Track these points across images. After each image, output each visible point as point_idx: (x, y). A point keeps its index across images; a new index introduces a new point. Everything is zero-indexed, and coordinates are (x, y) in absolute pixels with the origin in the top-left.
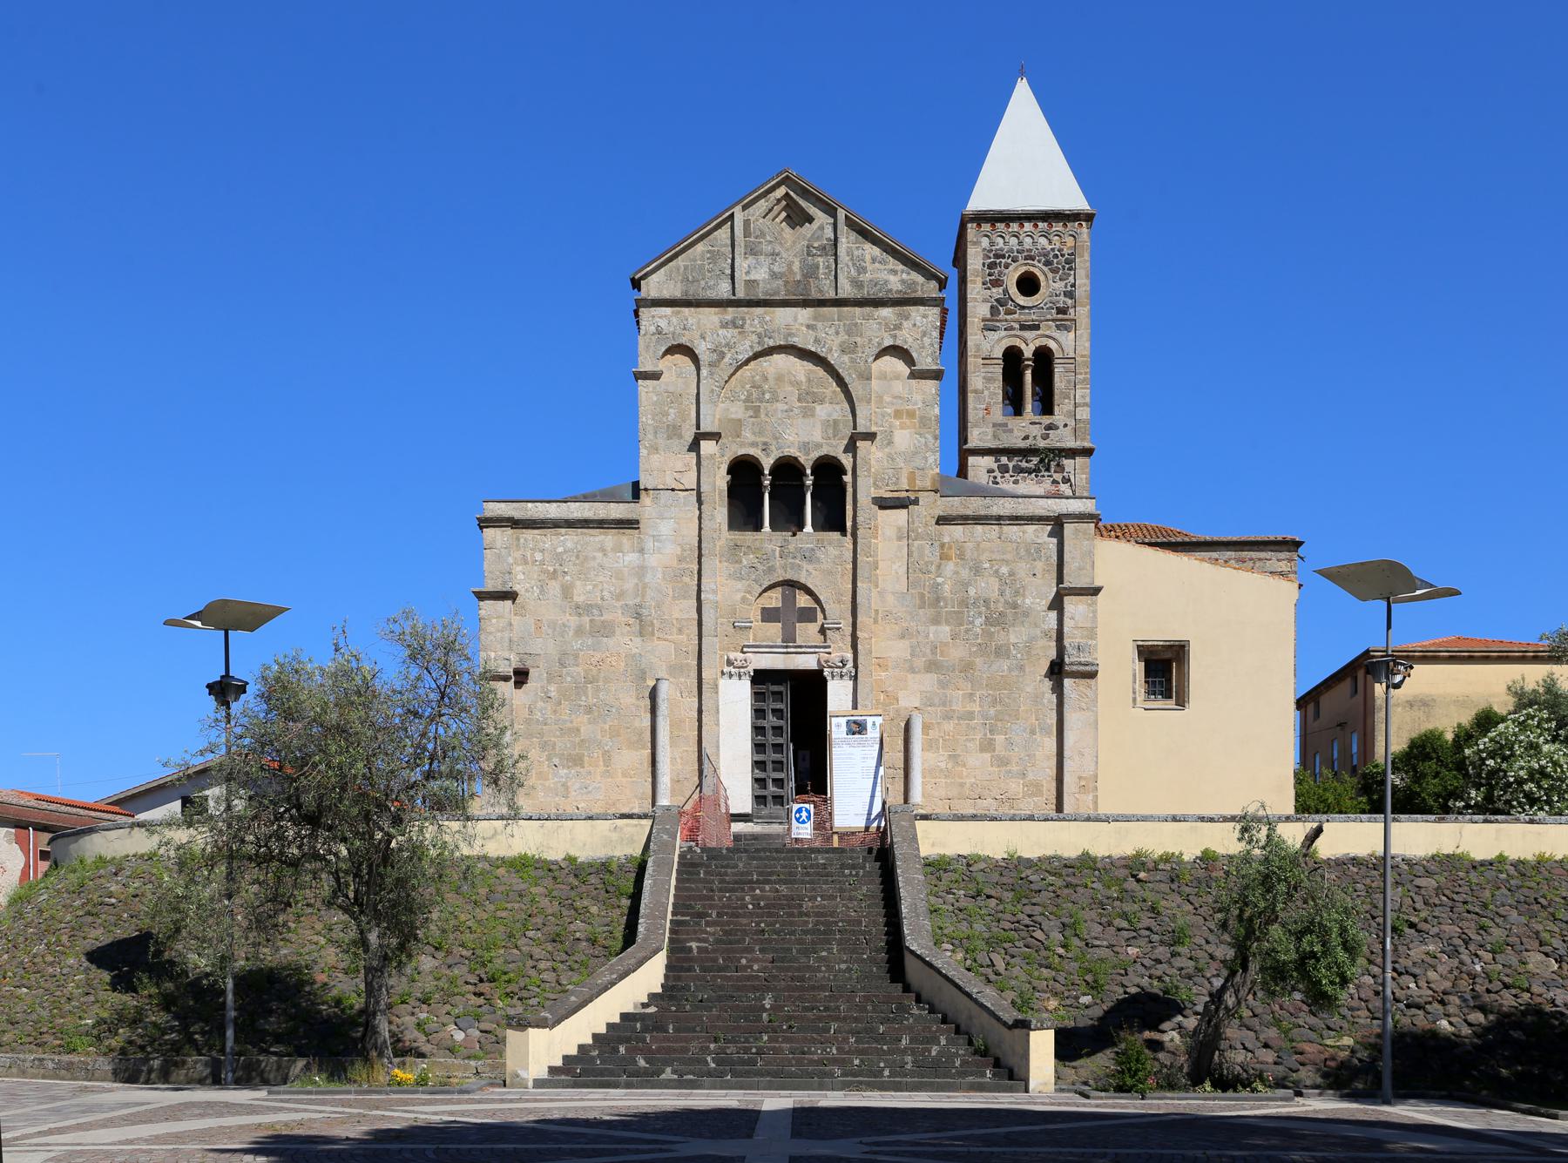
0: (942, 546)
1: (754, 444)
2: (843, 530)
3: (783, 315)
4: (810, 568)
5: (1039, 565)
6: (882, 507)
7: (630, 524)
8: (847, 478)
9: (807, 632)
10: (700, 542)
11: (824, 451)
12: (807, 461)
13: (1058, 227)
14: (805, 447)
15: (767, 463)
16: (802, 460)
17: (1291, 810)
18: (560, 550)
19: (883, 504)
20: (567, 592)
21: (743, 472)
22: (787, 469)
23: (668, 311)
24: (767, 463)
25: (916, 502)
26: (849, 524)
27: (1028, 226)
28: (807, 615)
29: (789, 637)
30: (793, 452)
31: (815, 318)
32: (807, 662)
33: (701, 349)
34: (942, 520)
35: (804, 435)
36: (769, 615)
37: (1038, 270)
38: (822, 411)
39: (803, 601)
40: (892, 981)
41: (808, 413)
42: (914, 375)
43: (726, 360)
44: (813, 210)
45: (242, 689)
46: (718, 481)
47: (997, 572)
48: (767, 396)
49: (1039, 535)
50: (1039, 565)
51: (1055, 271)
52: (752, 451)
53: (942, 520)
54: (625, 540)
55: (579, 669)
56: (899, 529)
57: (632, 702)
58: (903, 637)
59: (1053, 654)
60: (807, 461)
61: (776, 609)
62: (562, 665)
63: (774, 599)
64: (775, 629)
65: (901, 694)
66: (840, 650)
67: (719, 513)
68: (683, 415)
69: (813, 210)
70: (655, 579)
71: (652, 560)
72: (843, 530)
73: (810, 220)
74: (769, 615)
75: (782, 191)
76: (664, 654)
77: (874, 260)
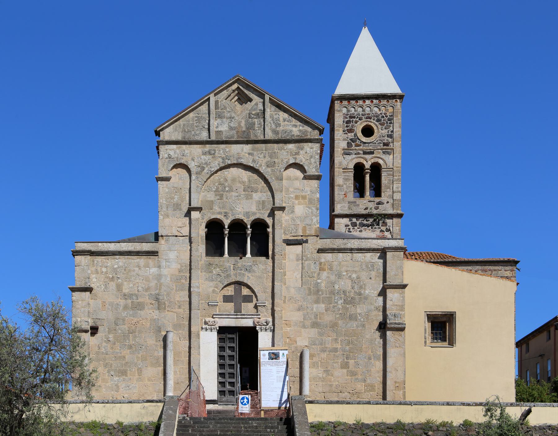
0: (321, 264)
1: (220, 213)
4: (249, 275)
5: (373, 273)
6: (288, 244)
7: (154, 253)
8: (270, 230)
9: (248, 307)
12: (248, 221)
13: (384, 102)
15: (227, 223)
16: (245, 221)
18: (116, 266)
19: (289, 243)
22: (238, 226)
24: (227, 223)
25: (306, 242)
26: (270, 253)
27: (368, 102)
28: (248, 299)
29: (238, 310)
30: (241, 217)
32: (248, 323)
33: (192, 165)
34: (320, 251)
37: (373, 124)
38: (256, 196)
39: (245, 292)
42: (305, 178)
43: (205, 171)
44: (252, 95)
46: (201, 231)
47: (350, 276)
48: (227, 189)
49: (374, 258)
50: (373, 273)
51: (382, 124)
52: (218, 217)
53: (320, 251)
55: (125, 326)
57: (153, 342)
58: (299, 310)
59: (381, 318)
60: (248, 221)
61: (231, 296)
62: (116, 324)
65: (298, 339)
66: (265, 316)
67: (201, 248)
69: (252, 95)
70: (166, 281)
71: (165, 271)
72: (267, 256)
73: (250, 100)
74: (227, 299)
75: (235, 86)
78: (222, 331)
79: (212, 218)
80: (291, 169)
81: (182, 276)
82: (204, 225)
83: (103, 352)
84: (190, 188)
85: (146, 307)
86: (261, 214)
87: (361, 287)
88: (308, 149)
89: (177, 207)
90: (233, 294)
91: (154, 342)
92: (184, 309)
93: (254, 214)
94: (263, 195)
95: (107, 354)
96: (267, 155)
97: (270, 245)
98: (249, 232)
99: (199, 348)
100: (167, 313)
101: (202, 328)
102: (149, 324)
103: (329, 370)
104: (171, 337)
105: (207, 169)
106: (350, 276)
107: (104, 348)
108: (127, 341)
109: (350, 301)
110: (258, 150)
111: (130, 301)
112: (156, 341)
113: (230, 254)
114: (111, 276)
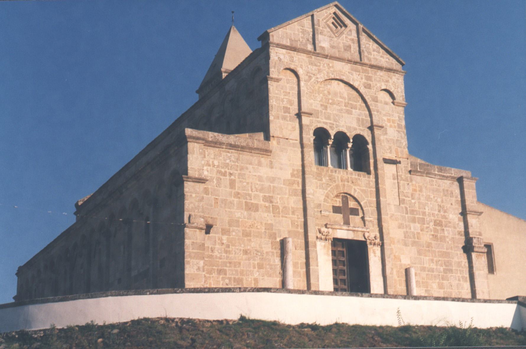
2: (369, 173)
3: (338, 65)
4: (356, 188)
5: (454, 199)
6: (385, 162)
7: (267, 152)
8: (370, 147)
9: (355, 220)
10: (303, 166)
11: (358, 132)
12: (351, 135)
14: (349, 128)
15: (332, 133)
16: (348, 134)
17: (332, 289)
19: (387, 161)
20: (232, 184)
21: (321, 135)
22: (341, 138)
23: (284, 51)
24: (332, 133)
25: (400, 162)
26: (372, 168)
28: (354, 212)
29: (347, 222)
30: (344, 130)
31: (352, 70)
33: (300, 72)
35: (351, 124)
36: (336, 210)
38: (356, 112)
39: (352, 204)
40: (16, 274)
41: (349, 112)
43: (312, 80)
44: (347, 21)
45: (346, 197)
46: (310, 138)
47: (436, 200)
48: (330, 101)
52: (325, 126)
54: (263, 160)
55: (240, 229)
56: (393, 175)
58: (399, 227)
60: (351, 135)
61: (339, 207)
62: (230, 225)
63: (338, 203)
64: (339, 217)
65: (402, 257)
66: (372, 233)
67: (311, 155)
68: (290, 102)
72: (369, 173)
73: (346, 26)
74: (336, 210)
76: (287, 226)
77: (374, 51)
78: (336, 242)
79: (319, 126)
80: (384, 92)
81: (294, 181)
82: (312, 132)
83: (216, 256)
84: (210, 290)
85: (260, 210)
86: (361, 130)
87: (445, 212)
88: (396, 80)
89: (287, 110)
90: (341, 205)
91: (270, 250)
92: (298, 216)
93: (355, 129)
94: (361, 112)
95: (221, 259)
96: (364, 77)
97: (372, 161)
98: (350, 145)
99: (317, 259)
100: (281, 218)
101: (317, 238)
102: (264, 228)
103: (430, 290)
104: (290, 246)
105: (314, 79)
106: (436, 200)
107: (218, 251)
108: (242, 246)
109: (438, 223)
110: (356, 71)
111: (244, 201)
112: (272, 249)
113: (170, 278)
114: (223, 170)
